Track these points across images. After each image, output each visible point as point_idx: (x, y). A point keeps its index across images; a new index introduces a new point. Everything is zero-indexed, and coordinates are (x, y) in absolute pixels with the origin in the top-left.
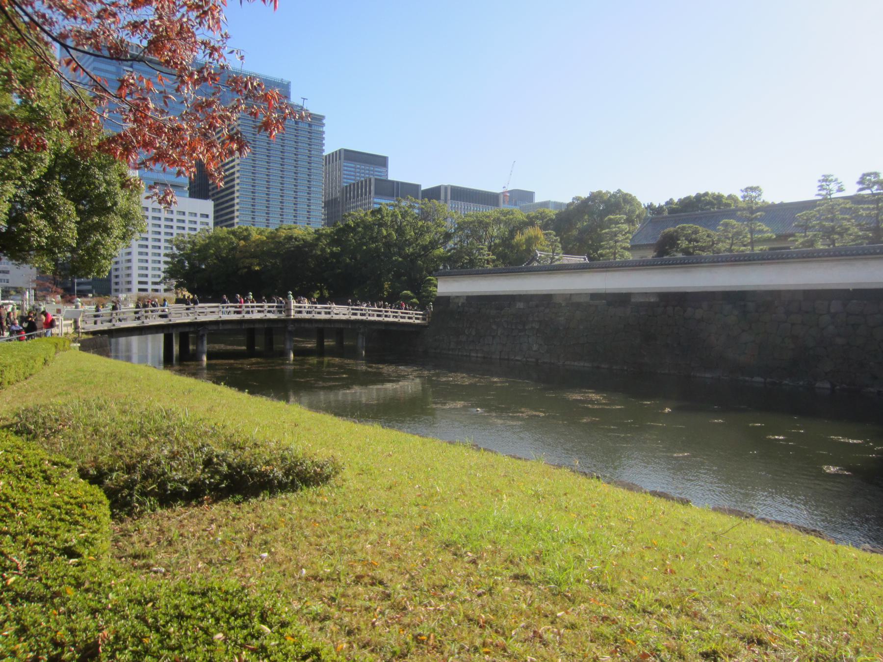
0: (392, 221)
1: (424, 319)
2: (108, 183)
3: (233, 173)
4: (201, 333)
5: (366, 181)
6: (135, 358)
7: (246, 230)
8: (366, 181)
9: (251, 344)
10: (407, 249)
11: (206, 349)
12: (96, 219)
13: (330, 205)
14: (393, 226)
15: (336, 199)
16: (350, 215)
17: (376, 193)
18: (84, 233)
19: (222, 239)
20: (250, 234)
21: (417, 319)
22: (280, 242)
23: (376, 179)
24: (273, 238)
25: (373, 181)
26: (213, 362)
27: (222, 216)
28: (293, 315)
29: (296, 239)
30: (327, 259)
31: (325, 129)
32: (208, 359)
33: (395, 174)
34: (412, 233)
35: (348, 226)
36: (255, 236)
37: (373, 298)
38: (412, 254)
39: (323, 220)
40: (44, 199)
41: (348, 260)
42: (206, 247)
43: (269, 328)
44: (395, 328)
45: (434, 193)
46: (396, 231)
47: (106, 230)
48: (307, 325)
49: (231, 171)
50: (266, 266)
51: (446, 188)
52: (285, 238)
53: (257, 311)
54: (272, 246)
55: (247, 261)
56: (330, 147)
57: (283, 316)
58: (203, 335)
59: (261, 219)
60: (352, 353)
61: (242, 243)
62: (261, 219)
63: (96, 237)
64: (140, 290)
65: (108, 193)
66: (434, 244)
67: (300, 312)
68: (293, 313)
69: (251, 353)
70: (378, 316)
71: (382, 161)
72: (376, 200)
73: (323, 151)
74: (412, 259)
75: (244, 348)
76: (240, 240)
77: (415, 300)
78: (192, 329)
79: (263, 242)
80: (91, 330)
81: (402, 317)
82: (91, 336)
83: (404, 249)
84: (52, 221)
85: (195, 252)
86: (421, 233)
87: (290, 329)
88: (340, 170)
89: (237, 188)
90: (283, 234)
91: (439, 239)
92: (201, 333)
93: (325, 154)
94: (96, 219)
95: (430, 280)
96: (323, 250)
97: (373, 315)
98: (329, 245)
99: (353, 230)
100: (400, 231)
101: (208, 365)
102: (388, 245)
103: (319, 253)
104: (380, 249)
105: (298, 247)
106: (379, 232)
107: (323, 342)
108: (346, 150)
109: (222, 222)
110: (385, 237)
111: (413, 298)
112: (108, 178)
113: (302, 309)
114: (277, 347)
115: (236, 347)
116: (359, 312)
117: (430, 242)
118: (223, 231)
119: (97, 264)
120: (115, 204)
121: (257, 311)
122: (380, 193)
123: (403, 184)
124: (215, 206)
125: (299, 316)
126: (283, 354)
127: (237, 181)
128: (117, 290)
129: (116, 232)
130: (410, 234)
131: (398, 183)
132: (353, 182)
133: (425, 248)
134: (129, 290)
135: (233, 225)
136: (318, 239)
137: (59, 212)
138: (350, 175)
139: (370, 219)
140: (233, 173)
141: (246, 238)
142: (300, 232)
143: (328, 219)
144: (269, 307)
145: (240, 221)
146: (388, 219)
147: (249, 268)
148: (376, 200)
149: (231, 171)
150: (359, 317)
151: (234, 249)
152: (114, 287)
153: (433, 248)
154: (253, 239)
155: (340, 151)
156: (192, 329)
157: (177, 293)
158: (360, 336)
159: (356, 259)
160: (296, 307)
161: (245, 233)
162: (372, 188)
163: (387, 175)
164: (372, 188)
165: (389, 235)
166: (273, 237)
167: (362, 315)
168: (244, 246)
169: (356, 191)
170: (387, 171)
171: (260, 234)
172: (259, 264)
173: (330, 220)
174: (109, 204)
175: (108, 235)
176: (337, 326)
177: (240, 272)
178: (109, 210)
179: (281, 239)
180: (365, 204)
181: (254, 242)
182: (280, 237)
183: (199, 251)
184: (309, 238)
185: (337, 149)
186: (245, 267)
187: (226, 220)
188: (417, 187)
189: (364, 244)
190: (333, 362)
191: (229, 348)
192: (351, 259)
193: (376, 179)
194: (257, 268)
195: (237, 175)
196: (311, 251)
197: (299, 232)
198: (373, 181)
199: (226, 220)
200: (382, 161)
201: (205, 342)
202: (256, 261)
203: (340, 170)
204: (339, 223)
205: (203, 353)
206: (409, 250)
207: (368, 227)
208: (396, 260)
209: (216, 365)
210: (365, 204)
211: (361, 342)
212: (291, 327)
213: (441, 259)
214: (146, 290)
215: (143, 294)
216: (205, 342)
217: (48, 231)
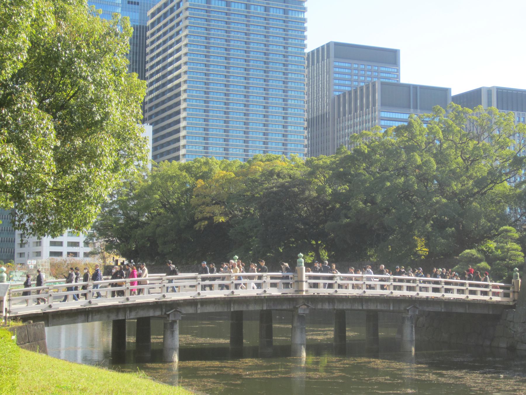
0: (428, 143)
1: (506, 295)
2: (99, 84)
3: (179, 85)
4: (171, 318)
5: (368, 88)
6: (63, 354)
7: (206, 163)
8: (368, 88)
9: (237, 335)
10: (454, 183)
11: (177, 344)
12: (78, 142)
13: (316, 124)
14: (429, 151)
15: (323, 116)
16: (362, 135)
17: (383, 104)
18: (64, 162)
19: (171, 178)
20: (211, 170)
21: (495, 294)
22: (256, 181)
23: (382, 84)
24: (245, 175)
25: (378, 86)
26: (190, 364)
27: (162, 146)
28: (306, 290)
29: (278, 175)
30: (326, 203)
31: (306, 15)
32: (181, 359)
33: (410, 74)
34: (460, 160)
35: (358, 152)
36: (218, 172)
37: (397, 260)
38: (462, 192)
39: (306, 146)
40: (13, 112)
41: (361, 205)
42: (149, 190)
43: (268, 311)
44: (461, 310)
45: (472, 98)
46: (435, 156)
47: (91, 156)
48: (326, 306)
49: (176, 82)
50: (235, 216)
51: (489, 91)
52: (263, 174)
53: (247, 283)
54: (244, 186)
55: (208, 209)
56: (314, 41)
57: (290, 292)
58: (174, 322)
59: (216, 149)
60: (393, 350)
61: (200, 183)
62: (216, 149)
63: (81, 168)
64: (52, 254)
65: (97, 99)
66: (495, 176)
67: (316, 286)
68: (305, 286)
69: (236, 351)
70: (435, 290)
71: (390, 57)
72: (383, 114)
73: (305, 46)
74: (462, 200)
75: (228, 341)
76: (197, 179)
77: (484, 264)
78: (158, 313)
79: (230, 181)
80: (21, 313)
81: (395, 288)
82: (20, 324)
83: (449, 185)
84: (21, 145)
85: (133, 199)
86: (472, 160)
87: (300, 311)
88: (328, 73)
89: (183, 105)
90: (259, 167)
91: (503, 167)
92: (171, 318)
93: (307, 51)
94: (78, 142)
95: (507, 231)
96: (321, 190)
97: (426, 289)
98: (329, 181)
99: (367, 158)
100: (441, 158)
101: (180, 368)
102: (423, 179)
103: (314, 194)
104: (412, 186)
105: (282, 185)
106: (410, 159)
107: (344, 332)
108: (337, 44)
109: (162, 155)
110: (419, 167)
111: (480, 261)
112: (97, 76)
113: (317, 281)
114: (278, 339)
115: (201, 340)
116: (405, 284)
117: (490, 173)
118: (169, 167)
119: (78, 213)
120: (106, 115)
121: (247, 283)
122: (389, 103)
123: (422, 88)
124: (155, 132)
125: (313, 292)
126: (287, 352)
127: (184, 96)
128: (21, 255)
129: (108, 161)
130: (457, 161)
131: (415, 87)
132: (349, 89)
133: (480, 183)
134: (38, 254)
135: (177, 158)
136: (312, 174)
137: (34, 132)
138: (343, 79)
139: (392, 139)
140: (179, 85)
141: (205, 176)
142: (285, 165)
143: (312, 145)
144: (272, 278)
145: (188, 153)
146: (422, 139)
147: (210, 219)
148: (383, 114)
149: (176, 82)
150: (479, 297)
151: (189, 191)
152: (18, 250)
153: (494, 182)
154: (216, 177)
155: (328, 45)
156: (158, 313)
157: (104, 258)
158: (408, 323)
159: (373, 202)
160: (310, 277)
161: (205, 169)
162: (378, 96)
163: (398, 77)
164: (378, 96)
165: (426, 163)
166: (243, 173)
167: (409, 289)
168: (204, 188)
169: (355, 101)
170: (398, 71)
171: (226, 168)
172: (225, 214)
173: (315, 147)
174: (98, 118)
175: (97, 165)
176: (372, 307)
177: (197, 226)
178: (97, 126)
179: (257, 176)
180: (367, 121)
181: (217, 181)
182: (255, 172)
183: (138, 197)
184: (298, 173)
185: (324, 42)
186: (205, 219)
187: (168, 152)
188: (445, 91)
189: (387, 179)
190: (372, 365)
191: (201, 340)
192: (365, 203)
193: (382, 84)
194: (222, 219)
195: (184, 87)
196: (303, 191)
197: (281, 165)
198: (378, 86)
199: (168, 152)
200: (390, 57)
201: (177, 332)
202: (217, 209)
203: (328, 73)
204: (345, 148)
205: (173, 349)
206: (456, 186)
207: (391, 153)
208: (437, 202)
209: (196, 369)
210: (367, 121)
211: (409, 333)
212: (302, 310)
213: (506, 198)
214: (60, 254)
215: (58, 259)
216: (177, 332)
217: (17, 163)
